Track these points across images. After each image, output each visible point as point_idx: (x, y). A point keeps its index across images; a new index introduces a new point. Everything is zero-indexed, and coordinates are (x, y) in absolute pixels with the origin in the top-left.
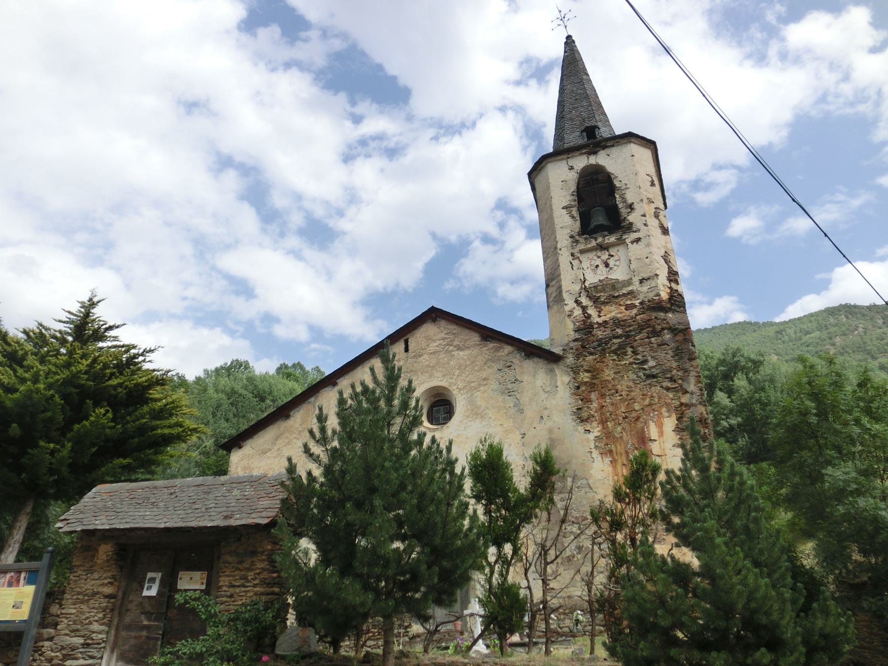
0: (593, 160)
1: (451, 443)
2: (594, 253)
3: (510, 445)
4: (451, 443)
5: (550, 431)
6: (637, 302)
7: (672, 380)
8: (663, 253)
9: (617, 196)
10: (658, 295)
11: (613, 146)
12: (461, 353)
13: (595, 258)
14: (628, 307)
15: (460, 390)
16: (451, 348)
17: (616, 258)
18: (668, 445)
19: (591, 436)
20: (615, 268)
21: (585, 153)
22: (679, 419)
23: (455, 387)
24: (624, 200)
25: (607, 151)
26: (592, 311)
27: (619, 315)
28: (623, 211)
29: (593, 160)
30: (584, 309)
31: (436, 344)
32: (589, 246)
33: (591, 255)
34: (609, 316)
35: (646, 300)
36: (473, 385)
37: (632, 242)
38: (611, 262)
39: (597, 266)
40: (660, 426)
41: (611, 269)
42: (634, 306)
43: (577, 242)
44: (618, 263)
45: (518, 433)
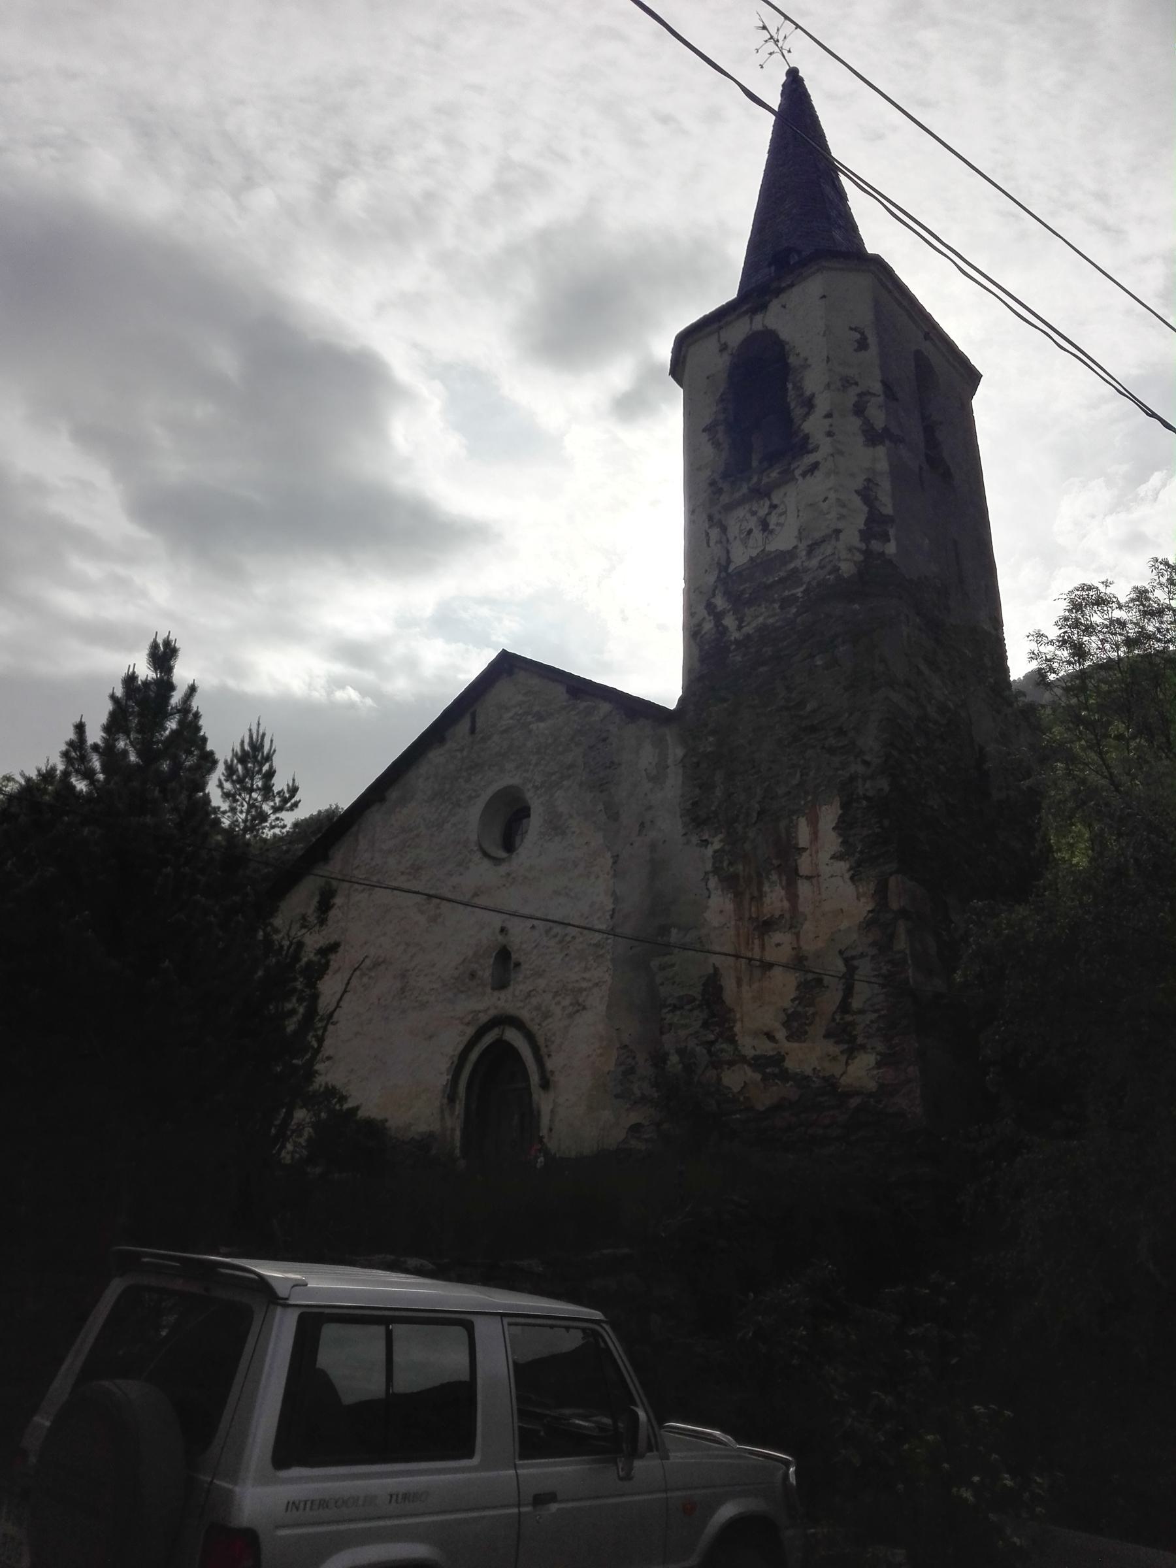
0: (758, 322)
1: (851, 329)
2: (747, 507)
3: (597, 877)
4: (851, 329)
5: (653, 847)
6: (799, 591)
7: (841, 732)
8: (859, 483)
9: (790, 386)
10: (836, 569)
11: (792, 285)
12: (542, 725)
13: (748, 516)
14: (785, 603)
15: (536, 788)
16: (529, 718)
17: (779, 510)
18: (824, 856)
19: (709, 852)
20: (778, 528)
21: (746, 313)
22: (845, 806)
23: (530, 786)
24: (799, 388)
25: (783, 297)
26: (729, 622)
27: (771, 621)
28: (798, 412)
29: (758, 322)
30: (718, 617)
31: (510, 714)
32: (737, 495)
33: (741, 512)
34: (754, 624)
35: (814, 583)
36: (554, 778)
37: (804, 475)
38: (773, 520)
39: (750, 532)
40: (814, 822)
41: (771, 532)
42: (794, 598)
43: (720, 491)
44: (782, 519)
45: (609, 854)
